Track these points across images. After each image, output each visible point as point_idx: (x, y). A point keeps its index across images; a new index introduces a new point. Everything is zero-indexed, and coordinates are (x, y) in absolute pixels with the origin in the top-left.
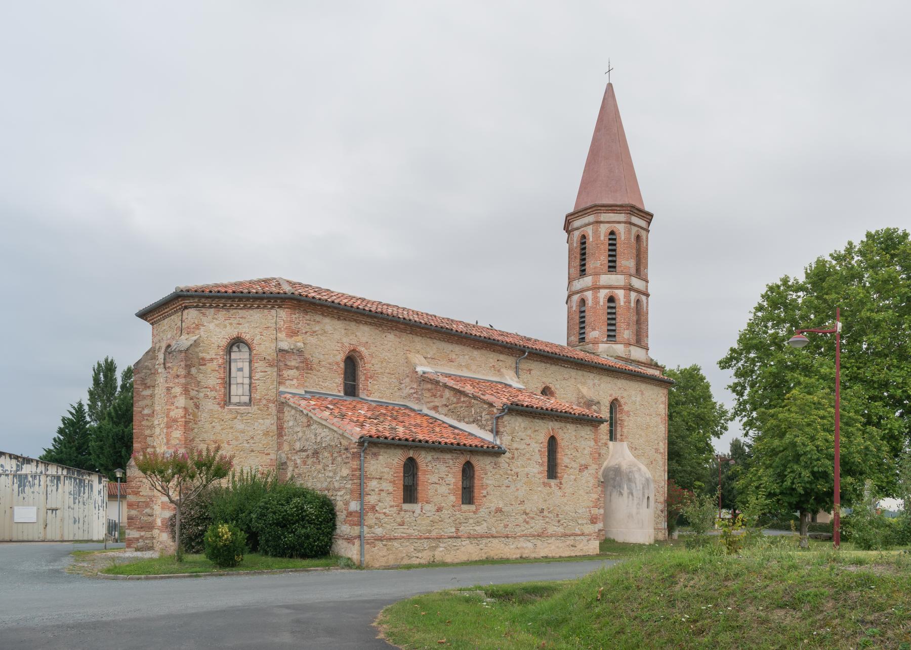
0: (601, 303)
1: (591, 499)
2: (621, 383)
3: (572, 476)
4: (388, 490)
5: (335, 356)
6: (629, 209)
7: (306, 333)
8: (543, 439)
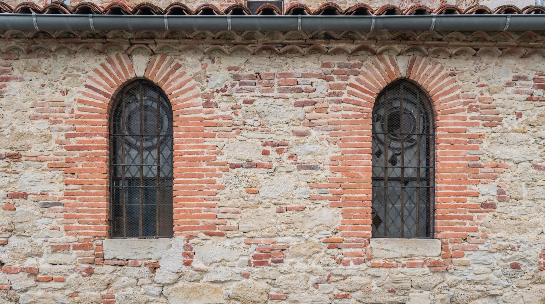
4: (43, 194)
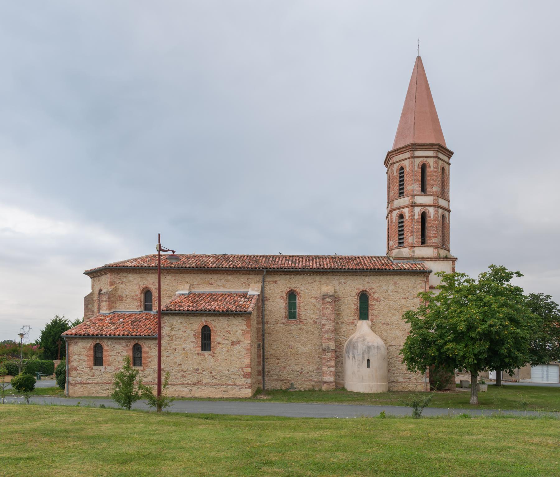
0: (394, 221)
1: (243, 363)
2: (368, 279)
3: (225, 349)
5: (135, 292)
6: (410, 147)
7: (119, 283)
8: (199, 328)
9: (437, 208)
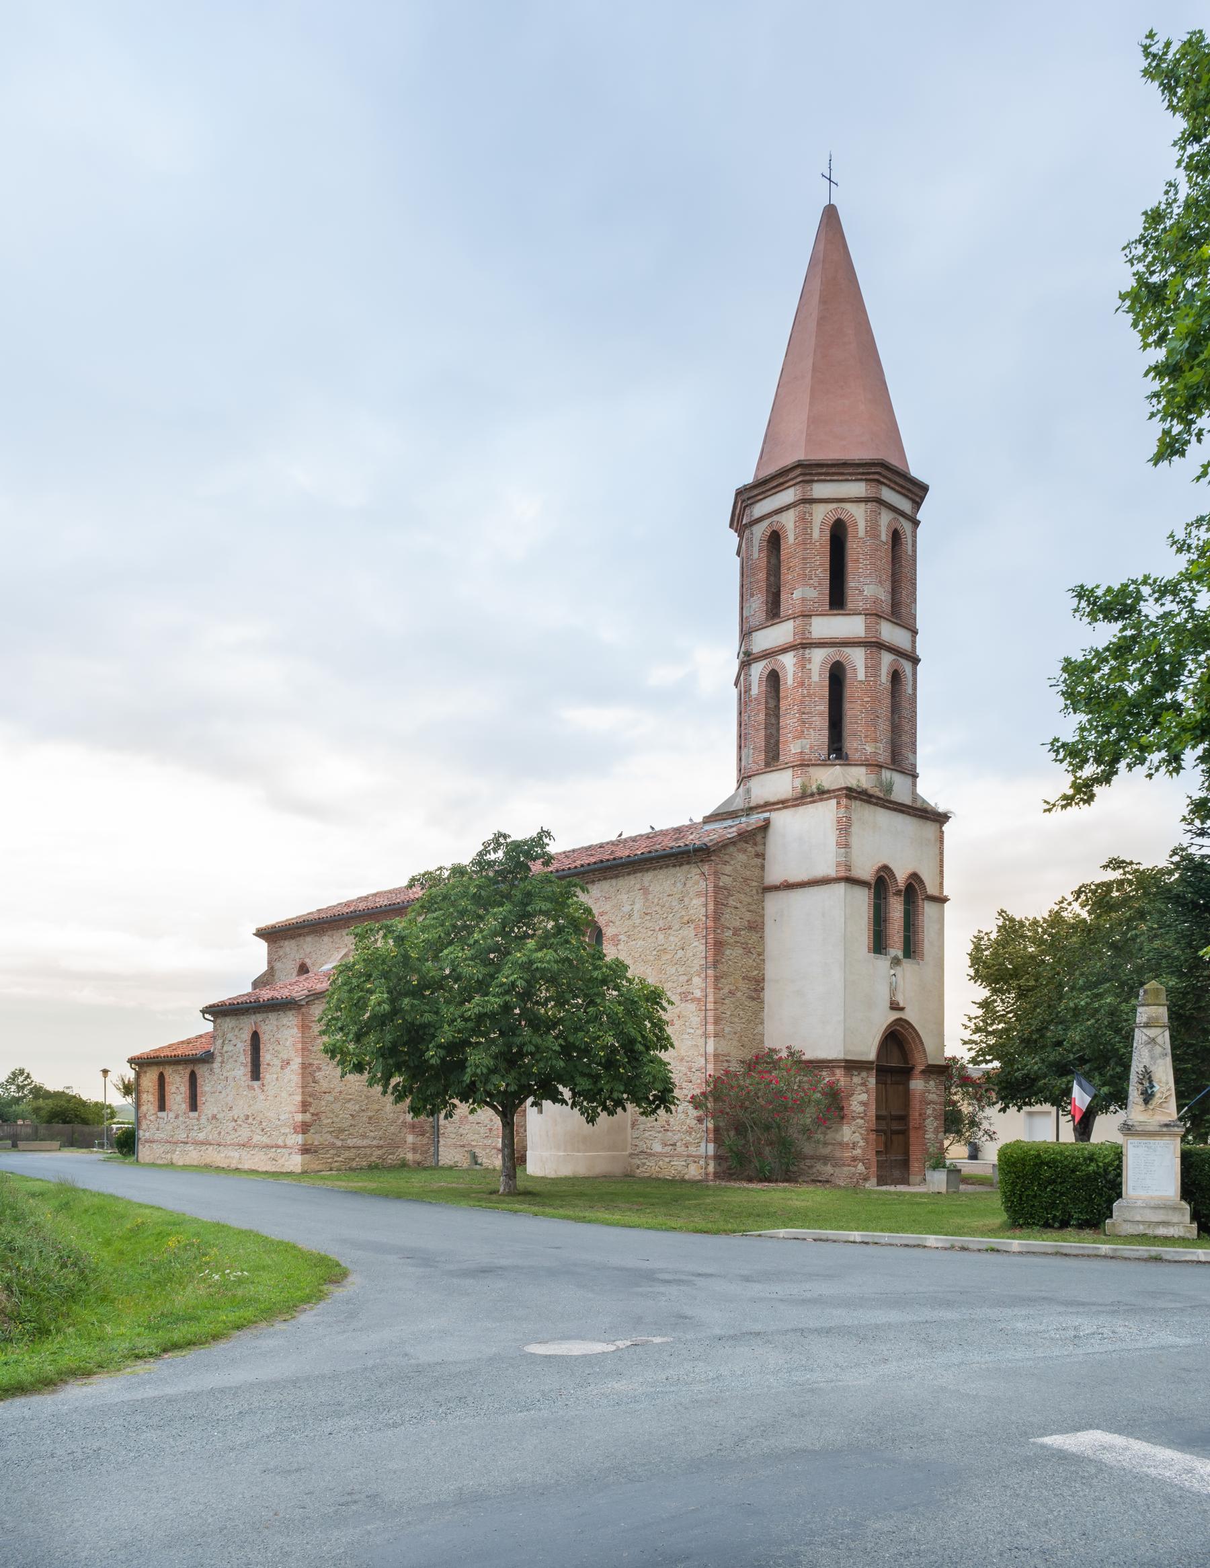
9: (801, 651)
